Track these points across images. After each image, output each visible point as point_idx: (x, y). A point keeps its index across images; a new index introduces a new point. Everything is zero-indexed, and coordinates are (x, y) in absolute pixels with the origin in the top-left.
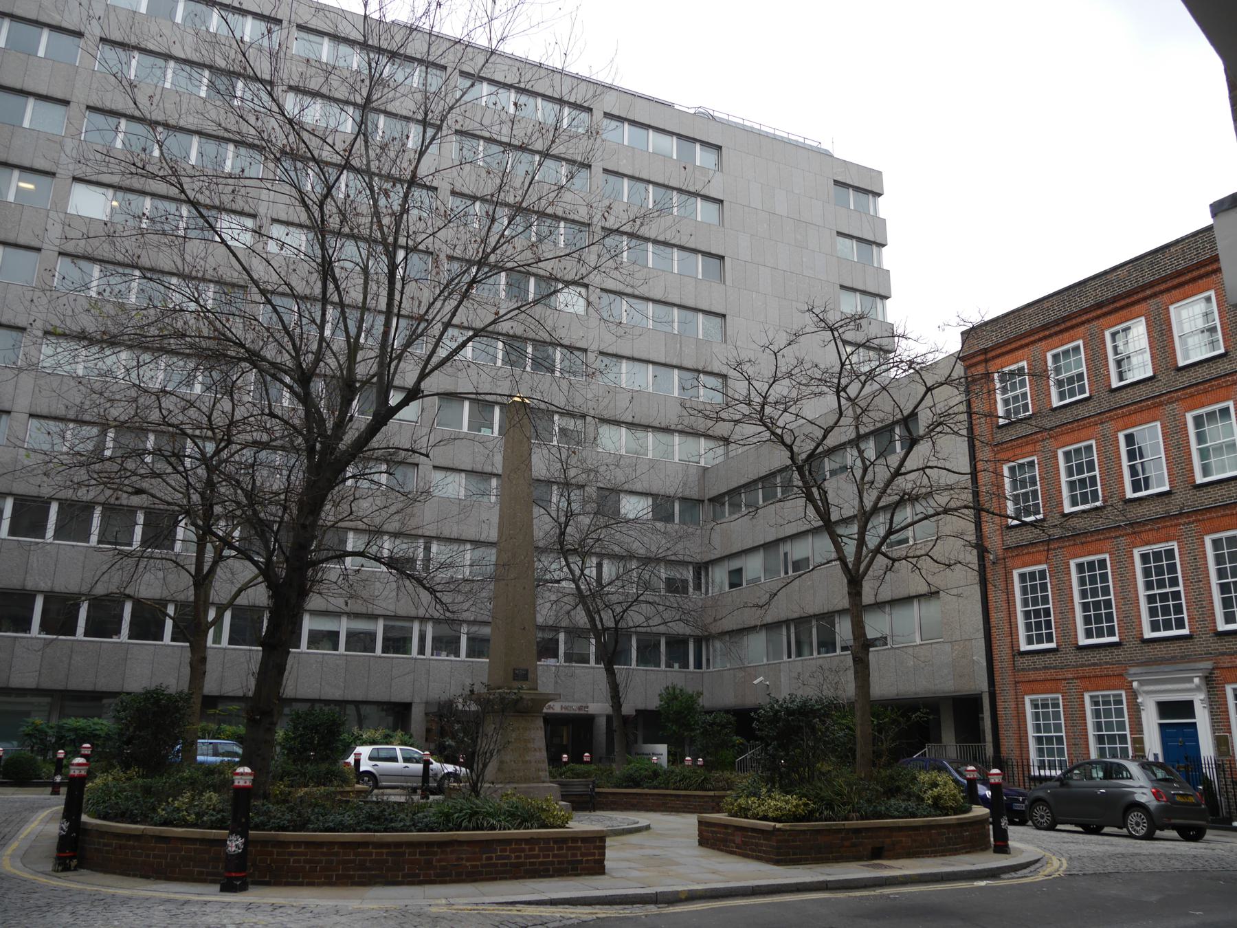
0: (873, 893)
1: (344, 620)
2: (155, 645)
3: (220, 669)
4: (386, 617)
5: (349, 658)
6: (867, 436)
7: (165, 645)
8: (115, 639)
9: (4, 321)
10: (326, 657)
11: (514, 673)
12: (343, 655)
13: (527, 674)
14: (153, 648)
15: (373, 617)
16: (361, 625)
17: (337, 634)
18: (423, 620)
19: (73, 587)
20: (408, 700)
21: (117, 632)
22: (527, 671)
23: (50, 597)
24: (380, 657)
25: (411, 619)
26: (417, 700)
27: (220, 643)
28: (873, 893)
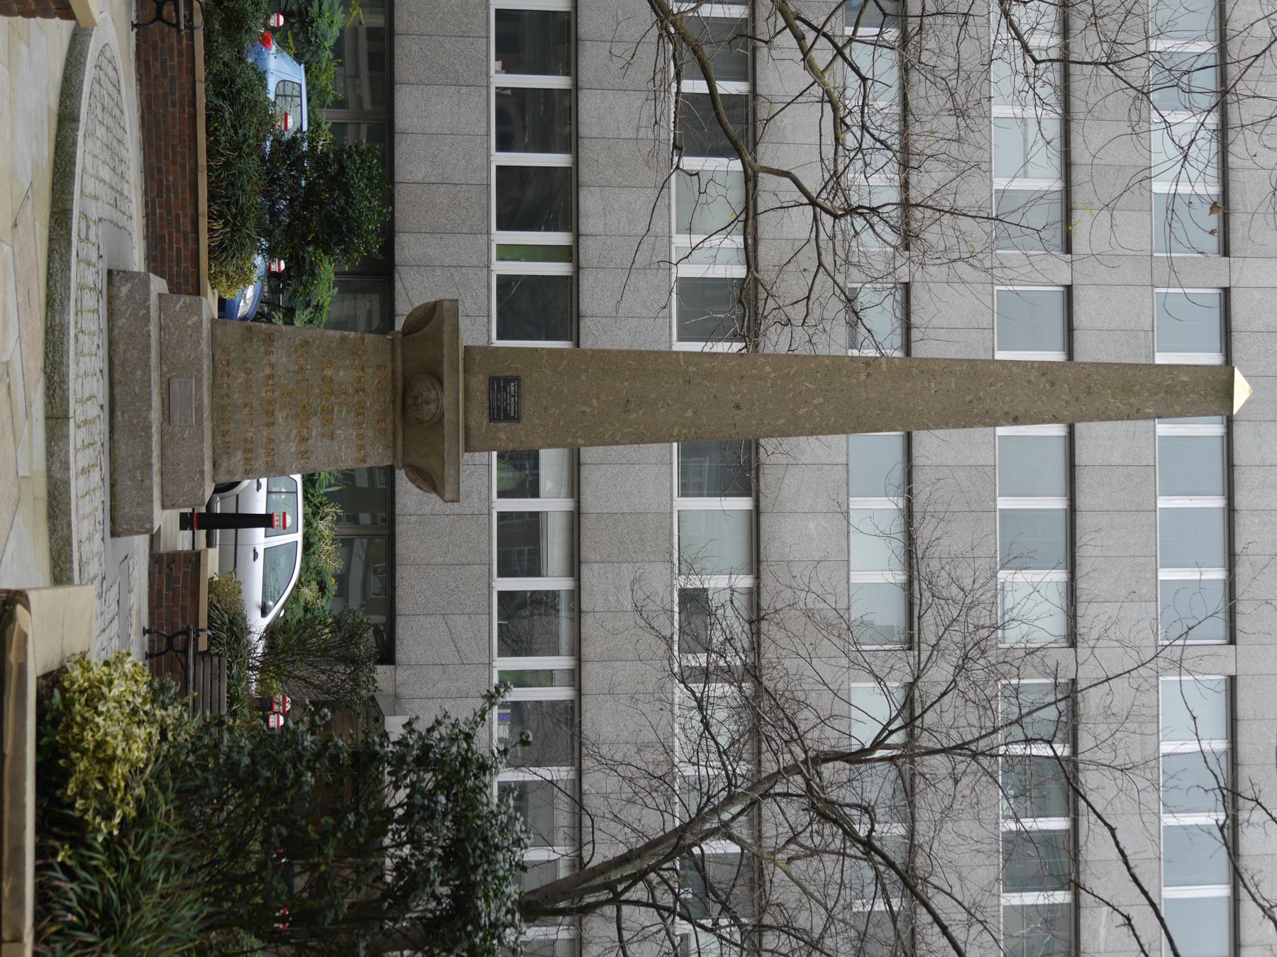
0: (205, 367)
1: (565, 504)
2: (488, 135)
3: (448, 261)
4: (576, 594)
5: (484, 519)
6: (1060, 700)
7: (488, 156)
8: (494, 65)
9: (1224, 947)
10: (483, 471)
11: (507, 381)
12: (490, 508)
13: (508, 418)
14: (483, 131)
15: (574, 566)
16: (554, 547)
17: (535, 493)
18: (575, 677)
19: (588, 224)
20: (399, 656)
21: (508, 68)
22: (517, 419)
23: (569, 99)
24: (490, 587)
25: (576, 651)
26: (402, 674)
27: (500, 258)
28: (205, 367)
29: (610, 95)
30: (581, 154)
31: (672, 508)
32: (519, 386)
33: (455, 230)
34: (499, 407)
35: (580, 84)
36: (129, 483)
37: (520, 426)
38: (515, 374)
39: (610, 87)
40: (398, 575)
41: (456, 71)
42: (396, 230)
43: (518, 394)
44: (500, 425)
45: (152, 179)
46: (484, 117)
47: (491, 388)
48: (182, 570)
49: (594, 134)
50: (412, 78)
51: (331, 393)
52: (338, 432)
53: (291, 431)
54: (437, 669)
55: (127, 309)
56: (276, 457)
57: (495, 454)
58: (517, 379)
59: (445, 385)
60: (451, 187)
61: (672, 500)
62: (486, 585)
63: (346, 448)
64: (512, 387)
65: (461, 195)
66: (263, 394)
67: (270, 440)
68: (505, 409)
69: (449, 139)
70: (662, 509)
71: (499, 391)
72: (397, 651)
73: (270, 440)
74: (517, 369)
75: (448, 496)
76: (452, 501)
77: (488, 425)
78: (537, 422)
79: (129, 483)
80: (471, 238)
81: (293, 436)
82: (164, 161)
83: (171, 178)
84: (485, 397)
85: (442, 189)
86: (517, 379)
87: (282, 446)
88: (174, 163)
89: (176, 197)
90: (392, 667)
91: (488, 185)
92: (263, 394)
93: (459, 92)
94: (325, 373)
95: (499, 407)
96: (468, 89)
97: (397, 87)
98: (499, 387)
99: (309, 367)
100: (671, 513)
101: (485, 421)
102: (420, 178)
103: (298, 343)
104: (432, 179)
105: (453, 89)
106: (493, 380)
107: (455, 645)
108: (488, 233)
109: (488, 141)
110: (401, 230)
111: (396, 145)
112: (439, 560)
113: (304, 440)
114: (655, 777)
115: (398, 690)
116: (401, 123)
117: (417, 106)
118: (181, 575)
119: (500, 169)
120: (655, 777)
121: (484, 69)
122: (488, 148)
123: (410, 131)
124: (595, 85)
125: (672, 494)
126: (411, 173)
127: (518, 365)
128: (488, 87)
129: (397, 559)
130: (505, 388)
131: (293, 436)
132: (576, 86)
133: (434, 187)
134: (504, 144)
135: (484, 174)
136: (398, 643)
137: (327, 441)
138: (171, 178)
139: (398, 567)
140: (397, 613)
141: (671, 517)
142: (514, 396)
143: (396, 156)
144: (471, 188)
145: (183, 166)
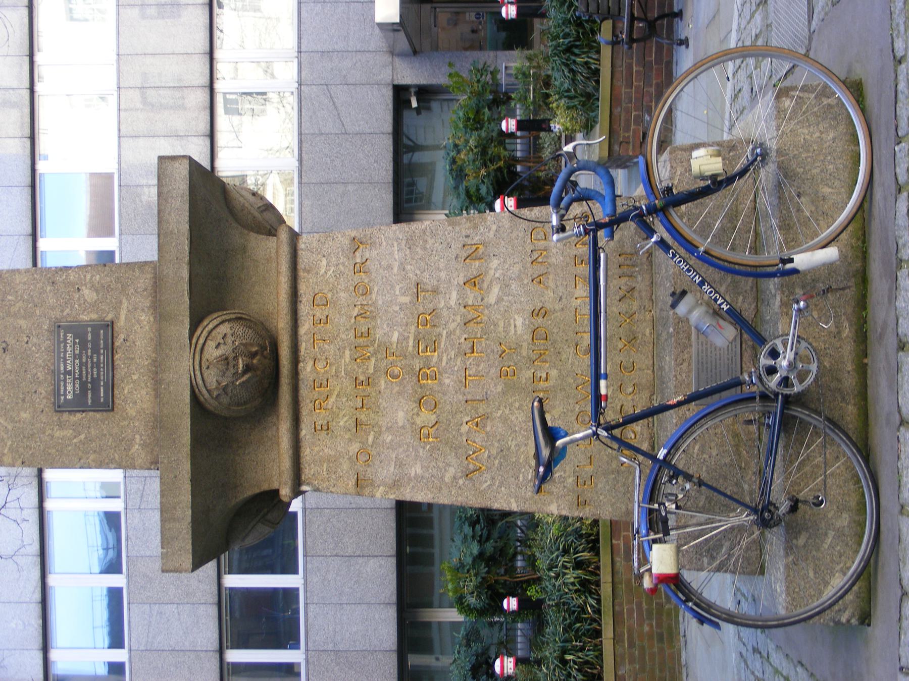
2: (306, 604)
7: (306, 584)
11: (79, 405)
13: (78, 330)
14: (311, 608)
20: (389, 93)
29: (187, 646)
30: (215, 588)
31: (120, 240)
32: (56, 393)
33: (337, 511)
34: (96, 350)
35: (217, 656)
36: (827, 190)
37: (57, 314)
38: (66, 416)
39: (187, 653)
40: (391, 172)
41: (338, 664)
42: (394, 511)
43: (57, 377)
44: (94, 316)
45: (670, 628)
46: (310, 621)
47: (111, 387)
48: (631, 134)
49: (202, 607)
50: (380, 656)
51: (419, 376)
52: (406, 299)
53: (499, 300)
54: (351, 81)
55: (832, 547)
56: (529, 248)
57: (117, 261)
58: (59, 408)
59: (824, 250)
60: (342, 553)
61: (120, 247)
62: (304, 162)
63: (389, 267)
64: (70, 390)
65: (331, 546)
66: (554, 373)
67: (539, 279)
68: (83, 347)
69: (344, 599)
70: (130, 238)
71: (95, 382)
72: (391, 98)
73: (539, 279)
74: (61, 426)
75: (182, 171)
76: (173, 158)
77: (117, 317)
78: (23, 323)
79: (827, 190)
80: (321, 505)
81: (496, 290)
82: (656, 650)
83: (646, 628)
84: (121, 371)
85: (350, 551)
86: (59, 408)
87: (516, 269)
88: (642, 648)
89: (639, 605)
90: (396, 83)
91: (305, 556)
92: (554, 373)
93: (335, 645)
94: (433, 418)
95: (96, 350)
96: (326, 647)
97: (395, 647)
98: (95, 390)
99: (464, 428)
100: (121, 234)
101: (121, 323)
102: (372, 561)
103: (487, 476)
104: (360, 560)
105: (341, 647)
106: (109, 406)
107: (334, 103)
108: (304, 510)
109: (306, 598)
110: (389, 511)
111: (395, 592)
112: (350, 188)
113: (472, 282)
114: (351, 183)
115: (390, 59)
116: (391, 613)
117: (375, 630)
118: (632, 127)
119: (295, 571)
120: (351, 183)
121: (311, 667)
122: (306, 591)
123: (382, 606)
124: (202, 655)
125: (121, 253)
126: (380, 566)
127: (58, 434)
128: (307, 650)
129: (391, 189)
130: (83, 386)
131: (496, 290)
132: (221, 652)
133: (358, 553)
134: (290, 594)
135: (309, 566)
136: (391, 106)
137: (429, 281)
138: (646, 628)
139: (391, 180)
140: (391, 136)
141: (121, 230)
142: (67, 373)
143: (395, 582)
144: (322, 553)
145: (631, 645)
